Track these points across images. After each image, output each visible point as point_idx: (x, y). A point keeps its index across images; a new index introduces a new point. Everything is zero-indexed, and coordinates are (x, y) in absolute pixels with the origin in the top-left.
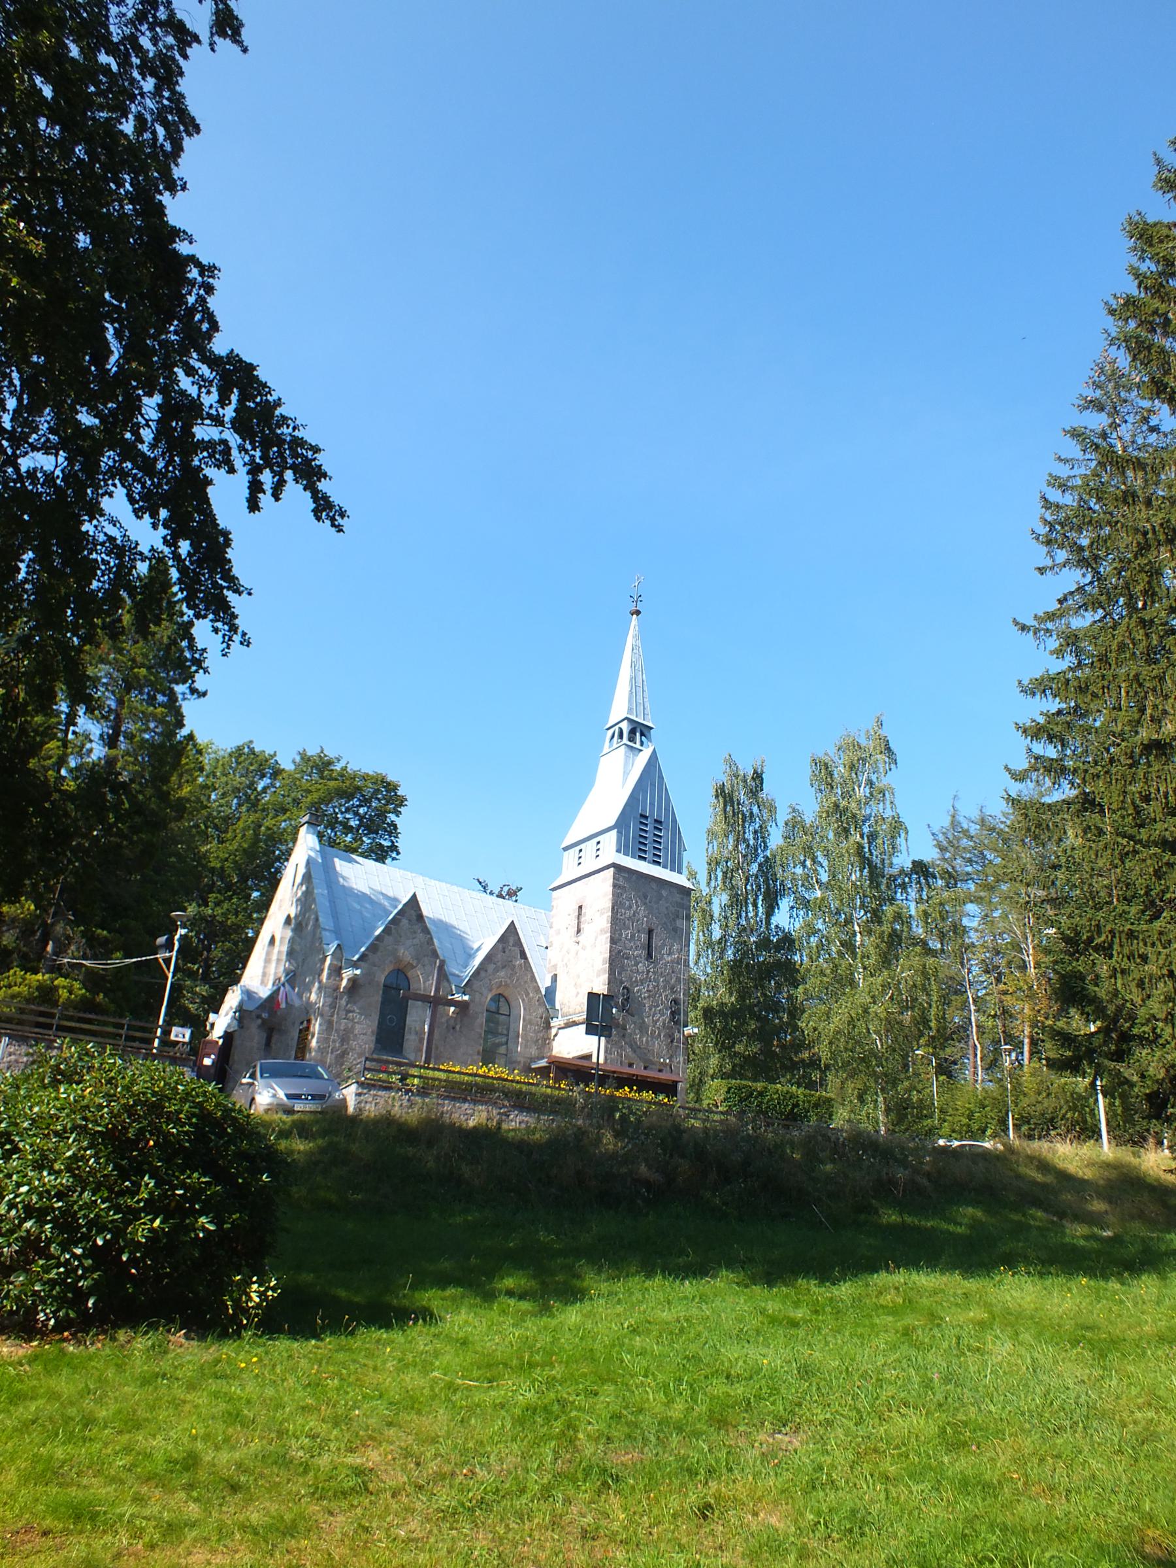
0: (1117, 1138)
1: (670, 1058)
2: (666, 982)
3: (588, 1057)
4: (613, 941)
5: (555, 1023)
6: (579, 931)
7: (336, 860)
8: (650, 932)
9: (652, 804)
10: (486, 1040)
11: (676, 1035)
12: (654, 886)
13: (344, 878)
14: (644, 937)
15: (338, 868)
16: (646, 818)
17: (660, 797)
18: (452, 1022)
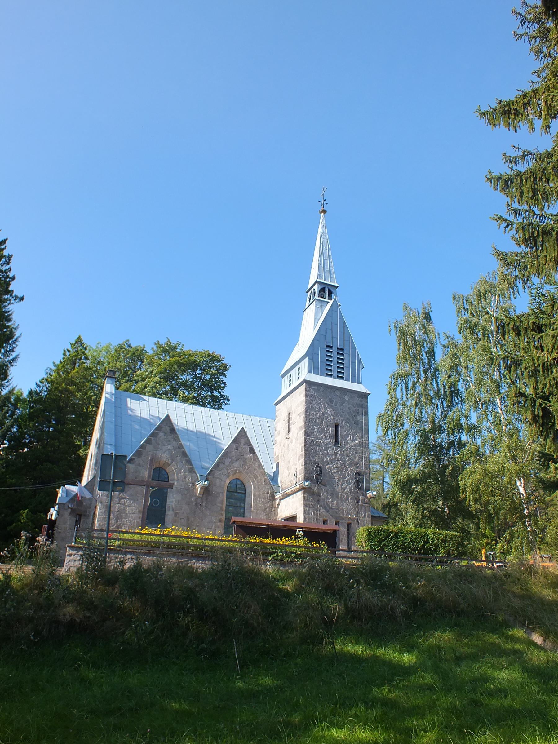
2: (351, 460)
3: (293, 518)
4: (307, 434)
5: (278, 496)
6: (289, 431)
7: (129, 400)
8: (337, 426)
11: (361, 498)
12: (338, 394)
13: (131, 409)
14: (332, 430)
15: (129, 405)
16: (331, 347)
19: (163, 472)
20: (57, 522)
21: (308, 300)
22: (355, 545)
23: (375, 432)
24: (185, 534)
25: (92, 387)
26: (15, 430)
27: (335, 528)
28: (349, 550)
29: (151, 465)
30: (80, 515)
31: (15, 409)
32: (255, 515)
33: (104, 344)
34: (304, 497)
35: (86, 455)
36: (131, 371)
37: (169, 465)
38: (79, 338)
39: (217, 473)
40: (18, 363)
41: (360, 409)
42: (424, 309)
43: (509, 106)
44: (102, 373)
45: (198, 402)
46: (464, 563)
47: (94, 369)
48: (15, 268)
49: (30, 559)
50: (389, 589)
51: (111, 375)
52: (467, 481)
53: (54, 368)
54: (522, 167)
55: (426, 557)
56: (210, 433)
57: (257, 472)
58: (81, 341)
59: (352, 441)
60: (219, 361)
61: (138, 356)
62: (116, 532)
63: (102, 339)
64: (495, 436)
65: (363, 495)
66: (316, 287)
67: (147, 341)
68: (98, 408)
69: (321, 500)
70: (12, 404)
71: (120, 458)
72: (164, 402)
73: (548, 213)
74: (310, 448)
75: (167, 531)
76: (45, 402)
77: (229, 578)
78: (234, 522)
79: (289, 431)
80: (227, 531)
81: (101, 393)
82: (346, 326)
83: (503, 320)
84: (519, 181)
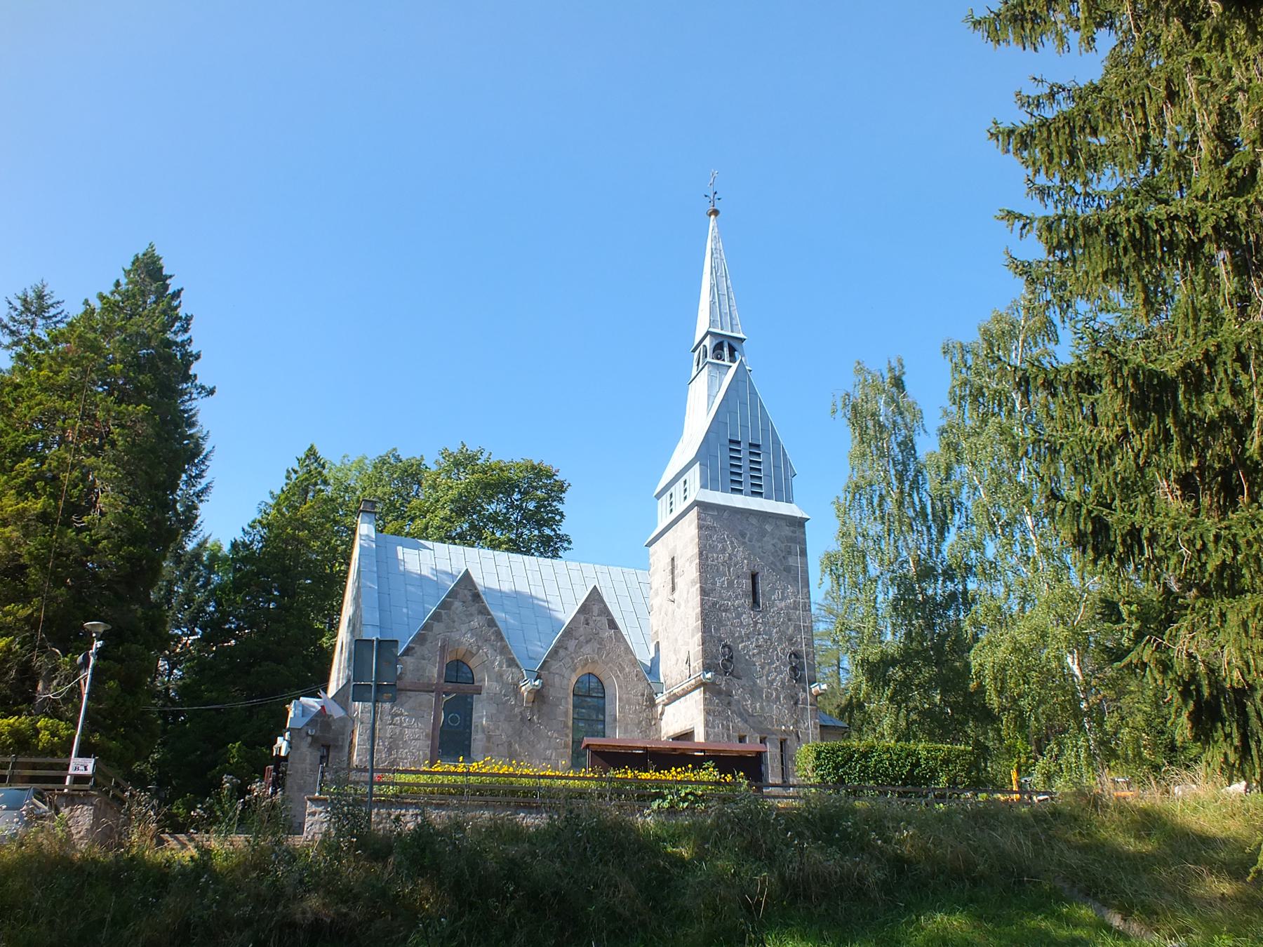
0: (106, 792)
2: (782, 633)
3: (688, 736)
4: (704, 592)
5: (660, 699)
6: (673, 589)
7: (399, 548)
8: (754, 577)
9: (744, 426)
11: (801, 695)
12: (754, 521)
14: (746, 583)
15: (401, 557)
16: (738, 443)
17: (754, 416)
19: (465, 669)
21: (695, 364)
22: (794, 776)
23: (820, 587)
24: (504, 770)
25: (338, 531)
26: (212, 609)
27: (760, 748)
28: (785, 785)
29: (442, 658)
30: (328, 747)
31: (210, 573)
32: (620, 735)
33: (354, 457)
34: (705, 699)
35: (334, 646)
36: (400, 501)
37: (473, 655)
39: (555, 666)
40: (211, 497)
42: (891, 369)
43: (1022, 6)
44: (353, 506)
45: (516, 547)
46: (982, 796)
47: (340, 500)
48: (200, 338)
49: (243, 824)
50: (854, 844)
51: (368, 507)
52: (983, 659)
53: (272, 502)
54: (1049, 112)
55: (917, 789)
56: (539, 596)
58: (314, 454)
59: (781, 600)
60: (550, 477)
61: (412, 474)
62: (389, 771)
63: (350, 450)
64: (1031, 595)
65: (805, 691)
66: (707, 342)
67: (427, 449)
68: (348, 565)
70: (204, 566)
71: (387, 646)
72: (458, 550)
73: (1098, 190)
74: (710, 616)
75: (474, 767)
76: (259, 559)
77: (579, 840)
78: (588, 746)
79: (673, 589)
80: (576, 763)
81: (353, 541)
82: (785, 454)
83: (1025, 371)
84: (1045, 135)
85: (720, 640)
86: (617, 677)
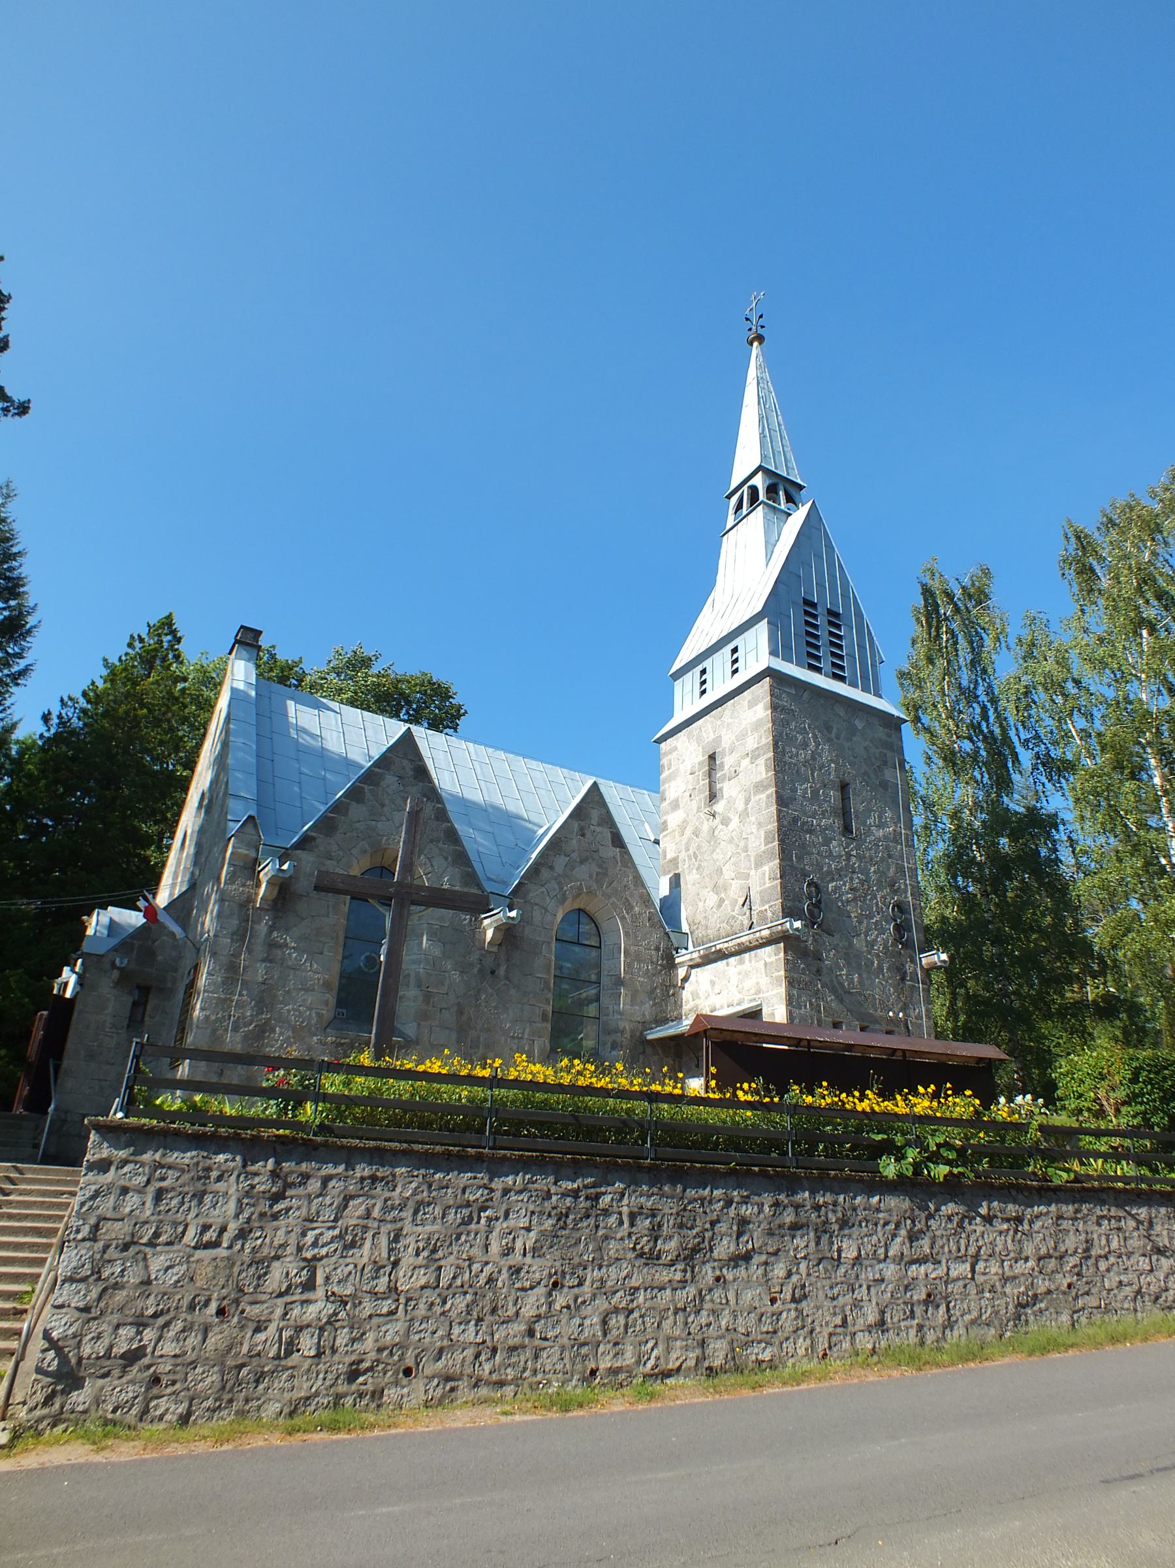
1: (904, 1009)
2: (881, 873)
3: (754, 1014)
4: (782, 801)
5: (682, 958)
7: (291, 704)
8: (844, 787)
9: (821, 585)
10: (559, 995)
11: (909, 967)
16: (814, 605)
18: (489, 962)
20: (78, 1006)
21: (731, 511)
34: (787, 962)
38: (169, 617)
40: (30, 681)
41: (889, 754)
53: (105, 672)
57: (632, 895)
58: (170, 624)
69: (825, 971)
74: (791, 836)
85: (805, 875)
86: (623, 918)
